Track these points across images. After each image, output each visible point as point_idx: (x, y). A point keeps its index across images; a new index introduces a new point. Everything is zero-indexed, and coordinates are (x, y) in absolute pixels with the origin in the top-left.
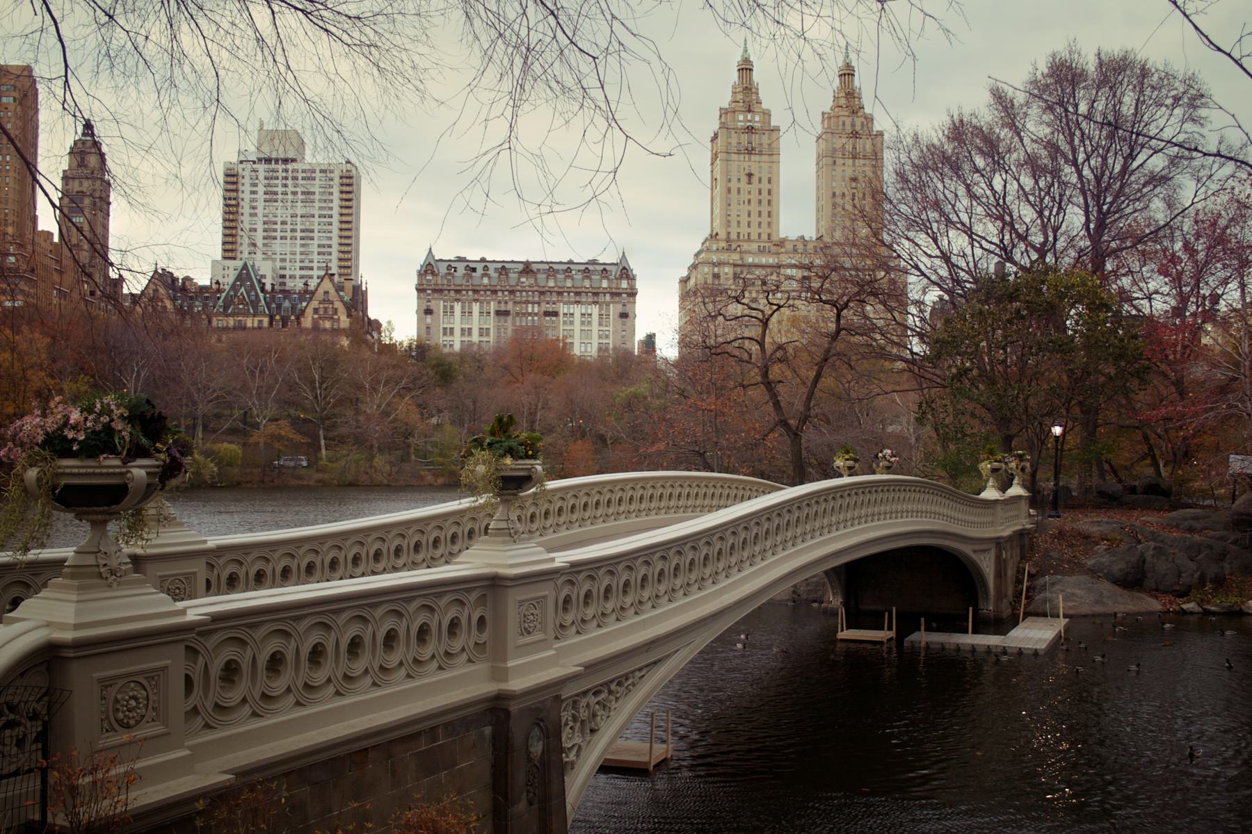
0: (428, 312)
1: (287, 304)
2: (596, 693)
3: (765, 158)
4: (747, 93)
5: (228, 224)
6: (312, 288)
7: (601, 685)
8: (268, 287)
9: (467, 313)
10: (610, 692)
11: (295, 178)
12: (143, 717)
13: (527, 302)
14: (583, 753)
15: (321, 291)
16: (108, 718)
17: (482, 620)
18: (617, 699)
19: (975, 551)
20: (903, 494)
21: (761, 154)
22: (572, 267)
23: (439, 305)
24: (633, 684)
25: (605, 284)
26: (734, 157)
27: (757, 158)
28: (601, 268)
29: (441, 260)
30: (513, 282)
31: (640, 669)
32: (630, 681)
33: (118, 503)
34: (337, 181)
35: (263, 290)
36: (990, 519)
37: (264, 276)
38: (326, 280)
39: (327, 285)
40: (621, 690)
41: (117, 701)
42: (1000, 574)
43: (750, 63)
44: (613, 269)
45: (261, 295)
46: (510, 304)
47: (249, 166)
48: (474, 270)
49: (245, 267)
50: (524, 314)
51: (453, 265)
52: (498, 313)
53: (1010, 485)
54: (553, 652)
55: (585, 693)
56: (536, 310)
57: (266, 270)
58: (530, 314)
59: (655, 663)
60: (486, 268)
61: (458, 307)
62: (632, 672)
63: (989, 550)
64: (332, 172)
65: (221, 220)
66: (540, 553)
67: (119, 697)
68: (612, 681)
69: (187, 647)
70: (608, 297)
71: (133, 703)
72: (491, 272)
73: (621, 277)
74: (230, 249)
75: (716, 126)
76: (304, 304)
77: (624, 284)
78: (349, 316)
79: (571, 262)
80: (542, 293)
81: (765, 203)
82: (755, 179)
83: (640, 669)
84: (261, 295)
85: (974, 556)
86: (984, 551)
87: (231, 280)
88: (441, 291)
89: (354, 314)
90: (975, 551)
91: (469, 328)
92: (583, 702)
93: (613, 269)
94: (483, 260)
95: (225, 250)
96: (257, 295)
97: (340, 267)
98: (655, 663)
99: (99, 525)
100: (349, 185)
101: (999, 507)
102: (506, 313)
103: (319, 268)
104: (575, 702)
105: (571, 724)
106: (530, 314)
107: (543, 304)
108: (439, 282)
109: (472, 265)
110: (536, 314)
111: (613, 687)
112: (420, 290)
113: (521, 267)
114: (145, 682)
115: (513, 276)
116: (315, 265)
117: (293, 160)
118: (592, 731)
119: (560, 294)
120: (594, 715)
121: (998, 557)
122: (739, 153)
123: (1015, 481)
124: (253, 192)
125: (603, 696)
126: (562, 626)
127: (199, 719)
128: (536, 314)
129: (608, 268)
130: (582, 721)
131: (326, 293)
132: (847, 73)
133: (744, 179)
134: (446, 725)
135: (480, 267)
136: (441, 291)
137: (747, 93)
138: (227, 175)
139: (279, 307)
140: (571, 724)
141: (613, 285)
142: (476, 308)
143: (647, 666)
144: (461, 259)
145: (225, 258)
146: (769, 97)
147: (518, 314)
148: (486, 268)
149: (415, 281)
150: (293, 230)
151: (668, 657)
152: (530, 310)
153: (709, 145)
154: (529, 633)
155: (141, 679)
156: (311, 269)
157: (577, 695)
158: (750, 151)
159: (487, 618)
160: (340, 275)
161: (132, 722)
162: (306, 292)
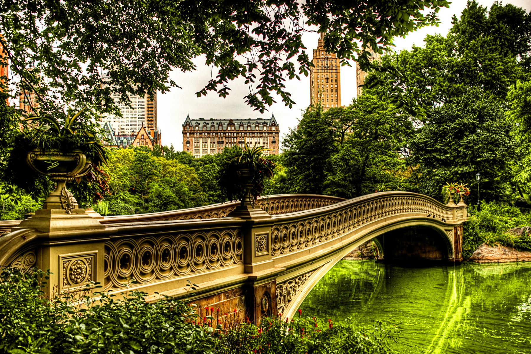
0: (188, 143)
1: (125, 140)
2: (290, 283)
3: (334, 71)
6: (136, 134)
7: (292, 279)
8: (116, 134)
10: (296, 283)
12: (84, 278)
13: (231, 137)
14: (285, 311)
15: (140, 134)
16: (66, 278)
17: (239, 244)
18: (299, 286)
19: (446, 230)
20: (415, 201)
21: (332, 69)
22: (251, 121)
23: (193, 140)
24: (306, 280)
25: (265, 128)
26: (320, 71)
28: (263, 121)
29: (193, 120)
30: (225, 129)
31: (308, 273)
32: (304, 278)
33: (71, 172)
35: (114, 134)
36: (451, 216)
38: (143, 129)
39: (143, 132)
40: (300, 282)
41: (71, 269)
42: (456, 242)
44: (268, 122)
45: (114, 137)
46: (224, 138)
48: (208, 124)
50: (230, 143)
51: (198, 122)
52: (218, 143)
53: (458, 202)
54: (271, 261)
55: (285, 282)
56: (235, 141)
58: (232, 143)
59: (314, 270)
60: (213, 123)
61: (201, 141)
62: (305, 274)
63: (451, 230)
66: (264, 213)
67: (73, 267)
68: (296, 277)
69: (105, 246)
70: (267, 134)
71: (79, 271)
72: (215, 125)
73: (272, 126)
76: (133, 140)
77: (273, 128)
78: (153, 145)
79: (250, 119)
82: (329, 81)
83: (308, 273)
84: (114, 137)
85: (445, 232)
89: (155, 144)
90: (446, 230)
91: (206, 149)
92: (284, 286)
93: (268, 122)
94: (211, 119)
96: (112, 137)
97: (148, 124)
98: (314, 270)
102: (222, 143)
104: (281, 286)
105: (279, 297)
106: (232, 143)
107: (238, 138)
109: (207, 122)
110: (235, 143)
111: (297, 280)
112: (184, 133)
113: (228, 122)
114: (85, 261)
115: (225, 126)
116: (137, 123)
118: (289, 301)
119: (245, 133)
120: (290, 294)
121: (456, 233)
122: (322, 69)
123: (461, 200)
125: (293, 284)
126: (275, 250)
127: (111, 282)
128: (235, 143)
129: (266, 121)
130: (284, 296)
133: (325, 81)
134: (225, 292)
135: (210, 122)
139: (122, 142)
140: (279, 297)
142: (209, 141)
143: (311, 271)
144: (201, 119)
147: (227, 143)
148: (213, 123)
149: (181, 129)
152: (232, 141)
155: (82, 259)
156: (135, 125)
157: (281, 283)
161: (79, 280)
162: (133, 135)
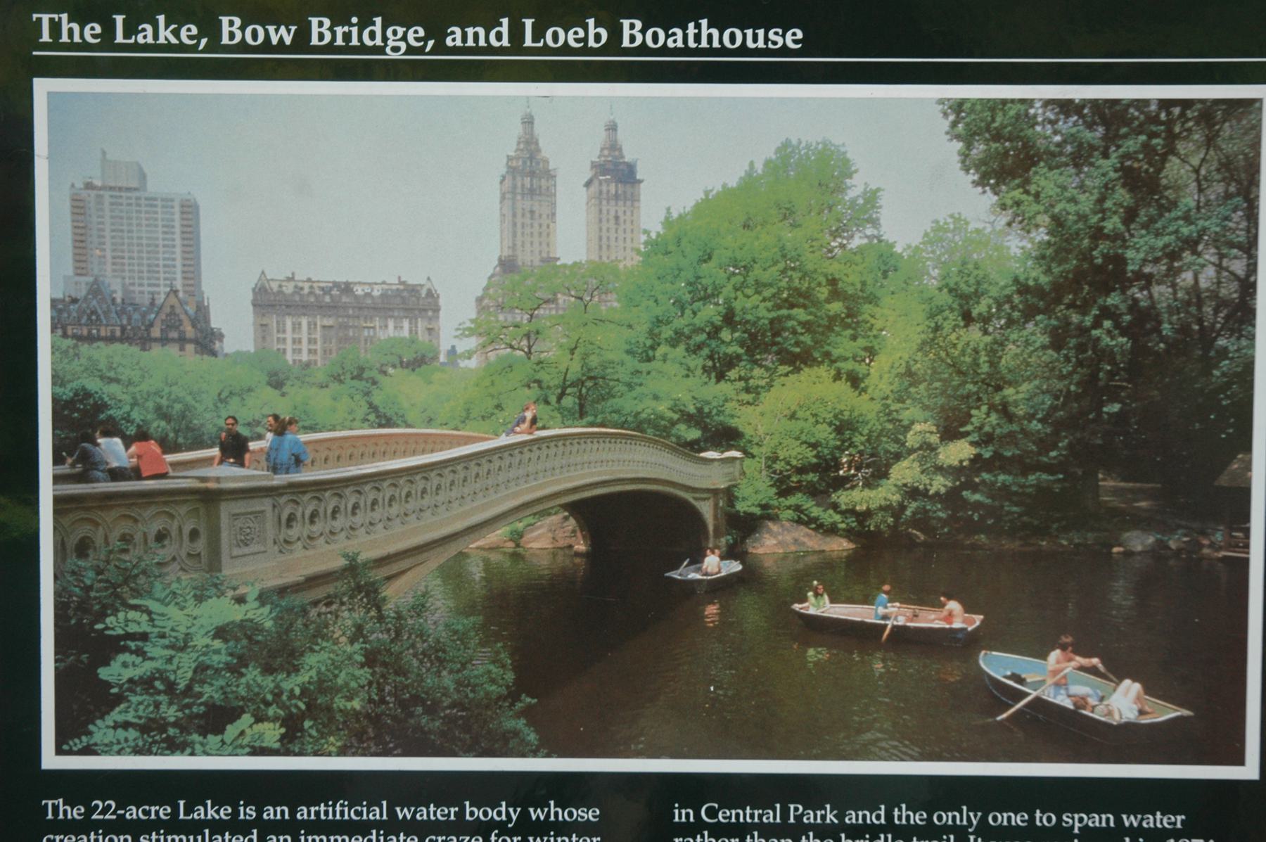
4: (529, 145)
5: (78, 258)
8: (119, 301)
9: (297, 327)
11: (138, 205)
21: (540, 194)
23: (273, 321)
27: (538, 198)
34: (177, 209)
37: (115, 292)
38: (172, 295)
43: (532, 117)
47: (93, 193)
48: (302, 289)
49: (96, 281)
57: (116, 288)
64: (172, 200)
65: (71, 248)
74: (80, 270)
75: (504, 170)
78: (194, 326)
80: (360, 308)
81: (544, 234)
86: (704, 499)
87: (84, 293)
88: (273, 306)
90: (696, 499)
95: (77, 268)
99: (737, 498)
100: (190, 210)
101: (716, 464)
103: (165, 285)
108: (270, 302)
109: (300, 284)
117: (136, 189)
124: (100, 237)
131: (172, 307)
132: (612, 128)
136: (273, 306)
137: (529, 145)
138: (73, 200)
141: (416, 302)
145: (78, 275)
146: (547, 149)
150: (138, 225)
151: (403, 572)
153: (498, 186)
154: (247, 545)
158: (532, 192)
159: (202, 530)
160: (185, 292)
